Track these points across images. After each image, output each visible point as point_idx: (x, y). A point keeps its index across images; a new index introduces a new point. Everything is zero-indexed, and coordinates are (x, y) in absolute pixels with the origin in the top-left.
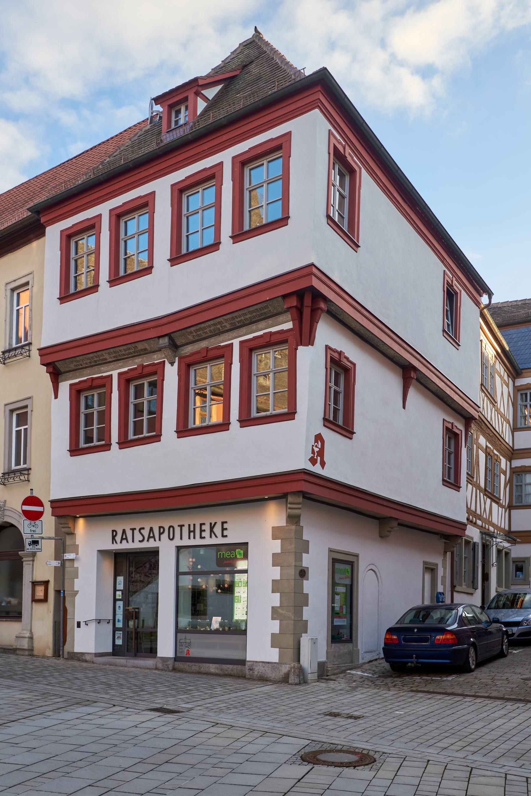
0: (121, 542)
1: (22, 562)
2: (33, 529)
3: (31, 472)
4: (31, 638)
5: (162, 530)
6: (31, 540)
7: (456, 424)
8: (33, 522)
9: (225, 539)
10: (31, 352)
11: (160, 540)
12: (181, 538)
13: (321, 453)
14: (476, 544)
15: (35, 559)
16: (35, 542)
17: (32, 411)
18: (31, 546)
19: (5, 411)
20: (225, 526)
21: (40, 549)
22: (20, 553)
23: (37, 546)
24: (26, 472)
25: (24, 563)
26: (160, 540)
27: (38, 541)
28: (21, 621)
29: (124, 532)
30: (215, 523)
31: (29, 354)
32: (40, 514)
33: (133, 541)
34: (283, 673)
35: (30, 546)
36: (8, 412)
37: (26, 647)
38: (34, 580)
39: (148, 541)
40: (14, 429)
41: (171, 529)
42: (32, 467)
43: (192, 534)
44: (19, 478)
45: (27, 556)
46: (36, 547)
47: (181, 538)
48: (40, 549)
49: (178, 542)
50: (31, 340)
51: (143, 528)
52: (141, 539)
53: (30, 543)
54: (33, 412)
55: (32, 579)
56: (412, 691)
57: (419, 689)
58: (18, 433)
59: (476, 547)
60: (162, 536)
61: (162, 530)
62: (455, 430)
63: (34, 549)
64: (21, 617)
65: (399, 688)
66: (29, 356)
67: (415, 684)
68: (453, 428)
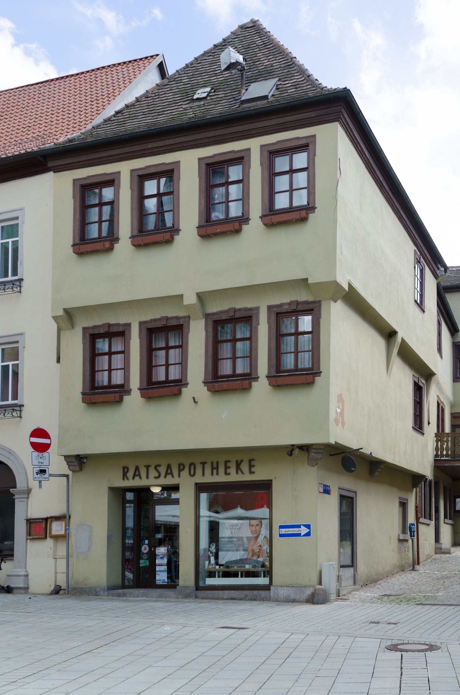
1: (14, 500)
2: (41, 460)
3: (24, 409)
4: (27, 576)
5: (182, 467)
6: (39, 469)
8: (41, 454)
9: (252, 475)
10: (22, 288)
11: (179, 476)
12: (203, 474)
15: (30, 495)
17: (24, 347)
18: (39, 475)
20: (253, 463)
21: (47, 478)
22: (11, 490)
23: (44, 475)
24: (18, 409)
25: (16, 501)
26: (179, 476)
28: (13, 560)
29: (137, 469)
30: (242, 461)
31: (20, 290)
33: (147, 477)
35: (37, 474)
37: (21, 585)
38: (29, 518)
41: (192, 467)
42: (24, 404)
43: (215, 471)
44: (12, 414)
45: (22, 492)
46: (44, 476)
47: (203, 474)
48: (47, 478)
49: (199, 479)
50: (22, 276)
51: (160, 465)
52: (157, 475)
53: (37, 471)
54: (25, 349)
60: (182, 473)
61: (182, 467)
62: (420, 384)
63: (41, 478)
66: (20, 292)
68: (419, 382)
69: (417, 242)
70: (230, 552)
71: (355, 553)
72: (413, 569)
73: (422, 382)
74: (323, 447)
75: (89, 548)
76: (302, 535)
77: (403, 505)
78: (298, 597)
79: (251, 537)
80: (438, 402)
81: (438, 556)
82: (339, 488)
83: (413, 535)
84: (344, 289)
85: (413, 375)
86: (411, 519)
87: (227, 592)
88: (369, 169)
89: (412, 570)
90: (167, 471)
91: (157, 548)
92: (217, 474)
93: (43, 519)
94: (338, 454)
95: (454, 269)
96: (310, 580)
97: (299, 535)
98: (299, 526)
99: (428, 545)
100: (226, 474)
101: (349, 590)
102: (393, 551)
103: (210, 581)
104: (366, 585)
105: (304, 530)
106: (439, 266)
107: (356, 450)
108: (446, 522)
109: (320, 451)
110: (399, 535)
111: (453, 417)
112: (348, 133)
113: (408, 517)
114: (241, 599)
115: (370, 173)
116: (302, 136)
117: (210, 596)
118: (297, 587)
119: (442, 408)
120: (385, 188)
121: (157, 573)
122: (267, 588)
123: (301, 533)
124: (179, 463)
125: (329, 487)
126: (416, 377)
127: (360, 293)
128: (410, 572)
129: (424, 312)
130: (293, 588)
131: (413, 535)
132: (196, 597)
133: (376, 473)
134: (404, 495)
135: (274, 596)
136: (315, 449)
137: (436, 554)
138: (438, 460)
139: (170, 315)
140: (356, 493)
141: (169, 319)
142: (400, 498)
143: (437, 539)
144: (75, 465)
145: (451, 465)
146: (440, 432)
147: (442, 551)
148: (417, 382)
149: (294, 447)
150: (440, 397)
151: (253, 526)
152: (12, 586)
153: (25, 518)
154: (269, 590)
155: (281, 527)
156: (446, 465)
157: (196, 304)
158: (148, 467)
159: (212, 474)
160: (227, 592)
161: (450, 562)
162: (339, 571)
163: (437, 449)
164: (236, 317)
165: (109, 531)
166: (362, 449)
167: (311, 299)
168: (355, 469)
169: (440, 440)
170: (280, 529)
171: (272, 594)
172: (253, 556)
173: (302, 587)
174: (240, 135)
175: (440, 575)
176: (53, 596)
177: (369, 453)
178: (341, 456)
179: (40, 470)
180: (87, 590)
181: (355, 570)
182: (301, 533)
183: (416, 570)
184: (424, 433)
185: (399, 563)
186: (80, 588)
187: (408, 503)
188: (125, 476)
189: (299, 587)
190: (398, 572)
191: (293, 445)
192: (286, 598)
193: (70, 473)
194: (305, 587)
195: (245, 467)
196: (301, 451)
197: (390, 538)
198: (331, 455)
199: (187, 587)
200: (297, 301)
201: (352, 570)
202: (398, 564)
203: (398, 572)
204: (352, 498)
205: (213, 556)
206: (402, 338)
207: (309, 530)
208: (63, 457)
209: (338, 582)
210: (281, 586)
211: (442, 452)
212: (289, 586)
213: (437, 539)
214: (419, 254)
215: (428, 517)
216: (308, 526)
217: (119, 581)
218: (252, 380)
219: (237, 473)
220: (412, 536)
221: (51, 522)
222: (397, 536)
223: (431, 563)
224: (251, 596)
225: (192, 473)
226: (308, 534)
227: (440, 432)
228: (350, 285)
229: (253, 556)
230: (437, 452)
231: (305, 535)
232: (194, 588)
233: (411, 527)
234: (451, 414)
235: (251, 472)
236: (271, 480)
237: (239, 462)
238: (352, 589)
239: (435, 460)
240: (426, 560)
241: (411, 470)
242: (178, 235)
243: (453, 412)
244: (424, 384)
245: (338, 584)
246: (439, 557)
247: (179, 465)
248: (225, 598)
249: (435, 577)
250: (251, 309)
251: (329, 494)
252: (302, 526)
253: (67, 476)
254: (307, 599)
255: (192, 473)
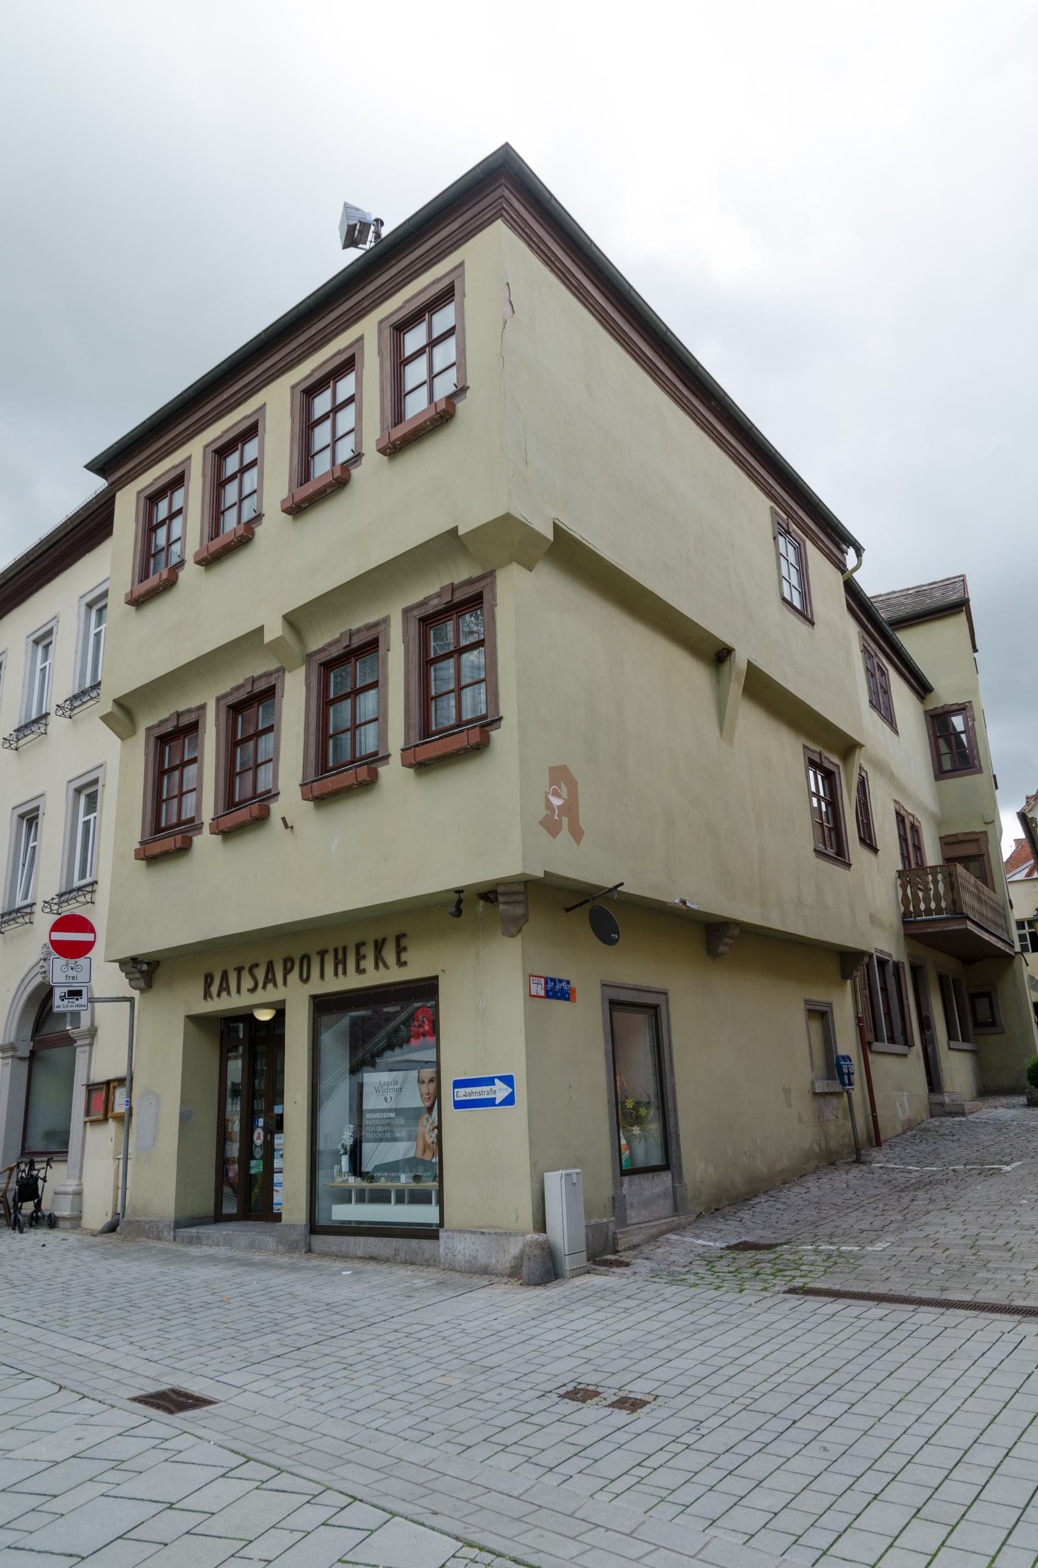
0: (219, 995)
2: (71, 973)
4: (79, 1194)
5: (289, 965)
6: (66, 990)
7: (826, 754)
8: (72, 961)
11: (285, 983)
12: (322, 976)
13: (571, 808)
14: (900, 965)
16: (76, 994)
18: (66, 1001)
19: (67, 792)
20: (404, 942)
23: (77, 999)
25: (78, 1050)
26: (285, 983)
27: (81, 991)
30: (384, 940)
32: (88, 946)
33: (239, 991)
34: (511, 1256)
35: (63, 1000)
36: (71, 792)
37: (66, 1213)
39: (264, 987)
40: (82, 819)
43: (340, 967)
46: (77, 1003)
47: (322, 976)
53: (63, 994)
55: (89, 1080)
56: (792, 1291)
57: (810, 1285)
58: (87, 823)
59: (901, 969)
62: (826, 764)
64: (67, 1152)
65: (765, 1280)
67: (802, 1267)
69: (773, 491)
70: (382, 1144)
71: (673, 1135)
72: (858, 1161)
73: (833, 760)
74: (521, 888)
75: (155, 1139)
76: (497, 1102)
77: (821, 1015)
78: (494, 1260)
79: (420, 1109)
80: (898, 813)
81: (935, 1122)
82: (604, 985)
83: (847, 1082)
84: (548, 540)
85: (805, 747)
86: (847, 1043)
87: (362, 1240)
88: (611, 330)
89: (854, 1162)
90: (266, 977)
91: (276, 1136)
92: (345, 973)
93: (102, 1083)
94: (580, 905)
95: (910, 592)
96: (517, 1217)
97: (490, 1102)
98: (489, 1081)
99: (905, 1100)
100: (360, 971)
101: (654, 1231)
102: (800, 1120)
103: (343, 1213)
104: (717, 1210)
105: (500, 1091)
106: (844, 547)
107: (611, 890)
108: (952, 1047)
109: (516, 898)
110: (813, 1083)
111: (946, 844)
112: (533, 245)
113: (835, 1043)
114: (387, 1260)
115: (616, 339)
116: (442, 275)
117: (334, 1249)
118: (490, 1234)
119: (913, 825)
120: (663, 374)
121: (275, 1188)
122: (429, 1233)
123: (495, 1099)
124: (284, 957)
125: (568, 982)
126: (814, 751)
127: (599, 552)
128: (848, 1167)
129: (812, 623)
130: (482, 1236)
131: (847, 1082)
132: (309, 1250)
133: (722, 949)
134: (819, 995)
135: (446, 1255)
136: (504, 894)
137: (932, 1116)
138: (910, 922)
139: (257, 673)
140: (665, 994)
141: (256, 680)
142: (807, 1002)
143: (934, 1081)
144: (137, 979)
145: (938, 929)
146: (907, 867)
147: (947, 1109)
148: (819, 761)
149: (462, 895)
150: (903, 804)
151: (423, 1082)
152: (57, 1213)
153: (85, 1082)
154: (437, 1238)
155: (458, 1084)
156: (929, 930)
157: (282, 636)
158: (239, 970)
159: (336, 974)
160: (362, 1239)
161: (956, 1138)
162: (618, 1185)
163: (905, 901)
164: (353, 646)
165: (184, 1101)
166: (621, 884)
167: (476, 572)
168: (618, 936)
169: (909, 882)
170: (456, 1090)
171: (442, 1250)
172: (424, 1152)
173: (501, 1234)
174: (345, 319)
175: (917, 1174)
176: (111, 1234)
177: (677, 901)
178: (587, 907)
179: (69, 991)
180: (147, 1226)
181: (678, 1177)
182: (495, 1099)
183: (863, 1163)
184: (851, 862)
185: (820, 1147)
186: (137, 1221)
187: (832, 1013)
188: (207, 995)
189: (495, 1234)
190: (817, 1168)
191: (459, 891)
192: (470, 1262)
193: (136, 994)
194: (508, 1234)
195: (389, 954)
196: (488, 904)
197: (787, 1091)
198: (568, 910)
199: (292, 1227)
200: (453, 584)
201: (666, 1178)
202: (817, 1149)
203: (817, 1168)
204: (655, 1008)
205: (345, 1153)
206: (749, 663)
207: (510, 1090)
208: (117, 964)
209: (614, 1216)
210: (460, 1231)
211: (916, 906)
212: (474, 1233)
213: (934, 1081)
214: (785, 517)
215: (901, 1039)
216: (508, 1080)
217: (208, 1206)
218: (379, 763)
219: (377, 967)
220: (846, 1085)
221: (115, 1088)
222: (808, 1085)
223: (912, 1140)
224: (406, 1253)
225: (305, 976)
226: (509, 1100)
227: (907, 867)
228: (557, 528)
229: (424, 1152)
230: (907, 907)
231: (502, 1103)
232: (306, 1230)
233: (841, 1065)
234: (941, 838)
235: (401, 964)
236: (436, 978)
237: (380, 942)
238: (664, 1227)
239: (904, 923)
240: (904, 1132)
241: (821, 938)
242: (261, 524)
243: (943, 835)
244: (838, 766)
245: (613, 1219)
246: (937, 1123)
247: (285, 961)
248: (359, 1255)
249: (901, 1180)
250: (376, 625)
251: (568, 999)
252: (496, 1080)
253: (131, 1000)
254: (511, 1267)
255: (305, 976)
